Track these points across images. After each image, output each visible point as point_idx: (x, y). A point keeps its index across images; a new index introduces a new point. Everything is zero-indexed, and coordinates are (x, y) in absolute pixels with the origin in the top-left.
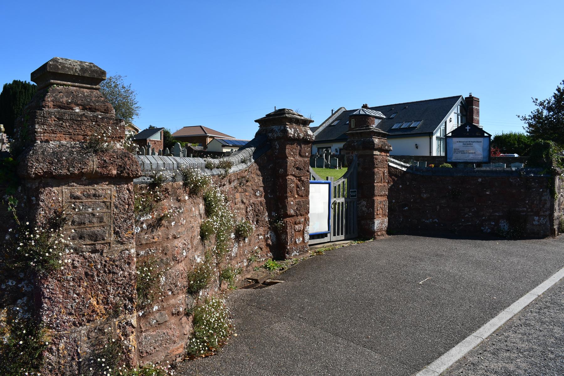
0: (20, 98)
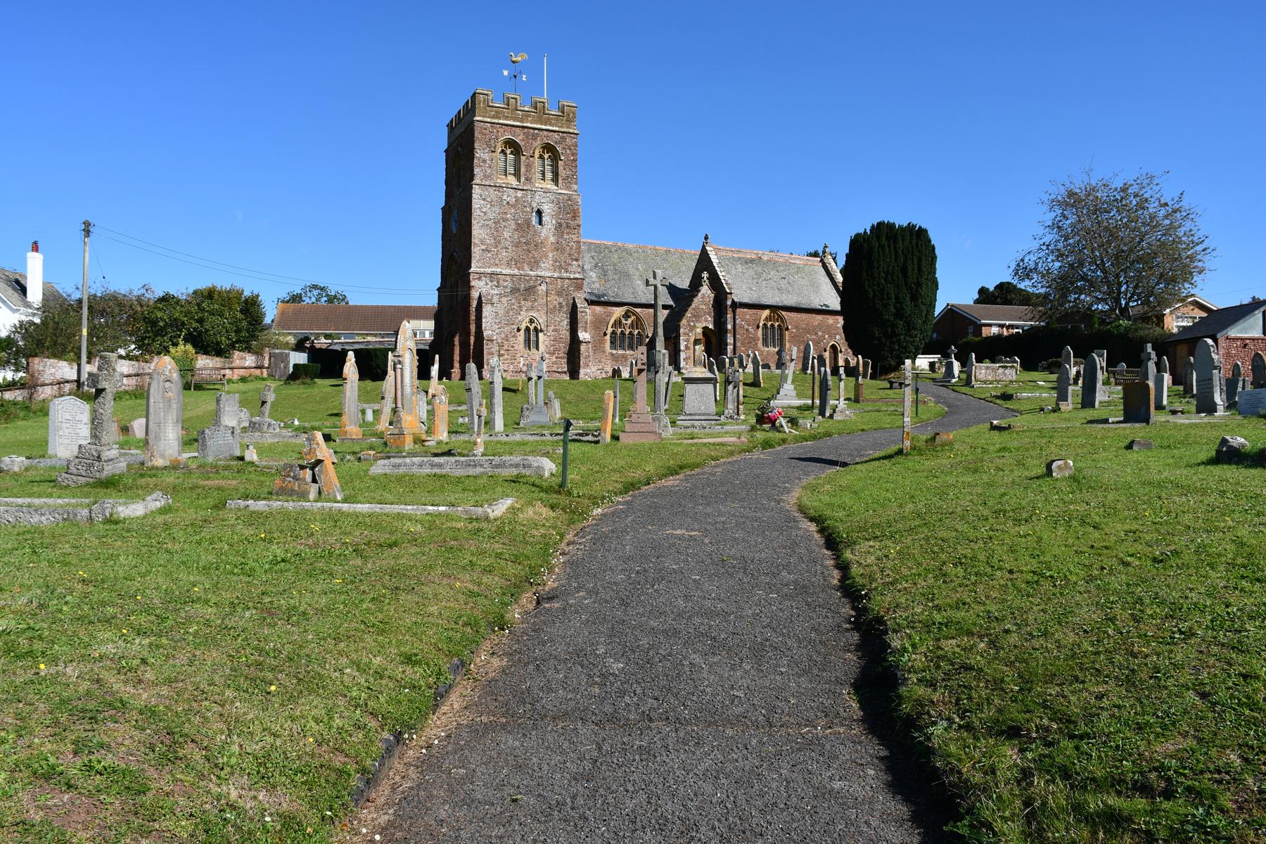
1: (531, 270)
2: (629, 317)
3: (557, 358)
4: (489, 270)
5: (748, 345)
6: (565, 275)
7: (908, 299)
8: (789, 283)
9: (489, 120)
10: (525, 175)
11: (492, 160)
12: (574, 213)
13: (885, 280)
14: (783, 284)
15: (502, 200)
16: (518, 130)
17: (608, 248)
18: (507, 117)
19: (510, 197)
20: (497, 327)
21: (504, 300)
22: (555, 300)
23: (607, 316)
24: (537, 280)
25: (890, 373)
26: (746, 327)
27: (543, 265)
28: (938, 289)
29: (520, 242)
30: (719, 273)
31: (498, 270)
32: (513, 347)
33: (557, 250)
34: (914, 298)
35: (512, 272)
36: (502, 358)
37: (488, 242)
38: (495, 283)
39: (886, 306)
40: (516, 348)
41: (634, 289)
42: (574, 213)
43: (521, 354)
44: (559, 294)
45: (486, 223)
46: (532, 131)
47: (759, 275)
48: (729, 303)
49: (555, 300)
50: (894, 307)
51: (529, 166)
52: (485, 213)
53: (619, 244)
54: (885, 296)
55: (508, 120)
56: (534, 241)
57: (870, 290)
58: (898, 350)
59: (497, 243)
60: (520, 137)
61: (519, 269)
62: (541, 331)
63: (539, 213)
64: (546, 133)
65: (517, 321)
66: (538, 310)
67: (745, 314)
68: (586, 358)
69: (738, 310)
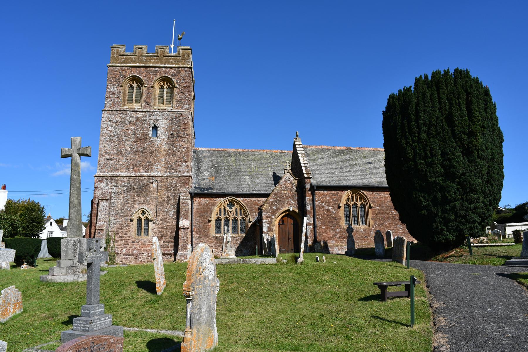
0: (417, 112)
1: (146, 172)
2: (234, 205)
3: (164, 242)
4: (110, 174)
5: (330, 224)
6: (174, 174)
7: (459, 154)
8: (375, 167)
9: (119, 65)
10: (145, 101)
11: (120, 92)
12: (185, 125)
13: (428, 134)
14: (368, 168)
15: (125, 121)
16: (142, 70)
17: (229, 153)
18: (134, 61)
19: (131, 117)
20: (113, 218)
21: (121, 197)
22: (164, 194)
23: (212, 205)
24: (149, 179)
25: (452, 249)
26: (326, 207)
27: (156, 167)
28: (502, 140)
29: (138, 151)
30: (302, 162)
31: (118, 174)
32: (126, 234)
33: (169, 155)
34: (467, 152)
35: (129, 174)
36: (116, 244)
37: (112, 152)
38: (114, 184)
39: (430, 165)
40: (129, 235)
41: (240, 182)
42: (185, 125)
43: (133, 240)
44: (168, 189)
45: (111, 138)
46: (153, 69)
47: (344, 162)
48: (308, 186)
49: (164, 194)
50: (443, 166)
51: (149, 94)
52: (111, 131)
53: (240, 150)
54: (429, 154)
55: (134, 63)
56: (149, 149)
57: (408, 148)
58: (456, 220)
59: (119, 152)
60: (144, 75)
61: (135, 172)
62: (151, 221)
63: (155, 128)
64: (164, 69)
65: (131, 213)
66: (149, 204)
67: (325, 196)
68: (184, 242)
69: (317, 193)
